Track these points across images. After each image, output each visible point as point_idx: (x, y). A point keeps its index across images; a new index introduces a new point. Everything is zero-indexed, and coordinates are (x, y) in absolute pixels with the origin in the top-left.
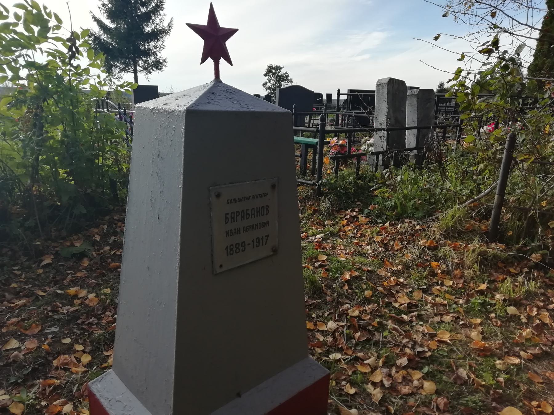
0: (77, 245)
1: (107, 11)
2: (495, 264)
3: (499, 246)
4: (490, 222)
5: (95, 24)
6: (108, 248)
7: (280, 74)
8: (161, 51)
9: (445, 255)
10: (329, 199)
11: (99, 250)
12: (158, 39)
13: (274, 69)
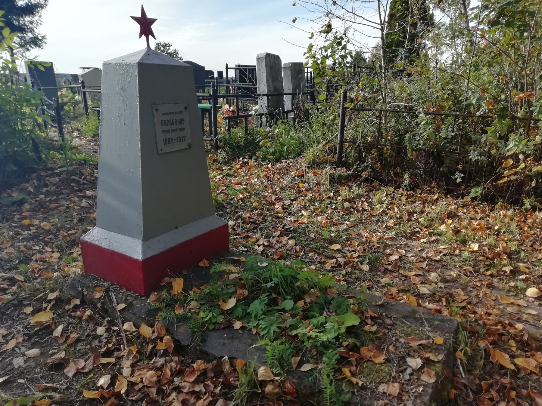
0: (15, 195)
2: (340, 182)
3: (342, 169)
6: (42, 196)
7: (169, 51)
8: (38, 27)
9: (308, 180)
10: (225, 151)
11: (35, 198)
12: (33, 14)
13: (162, 46)
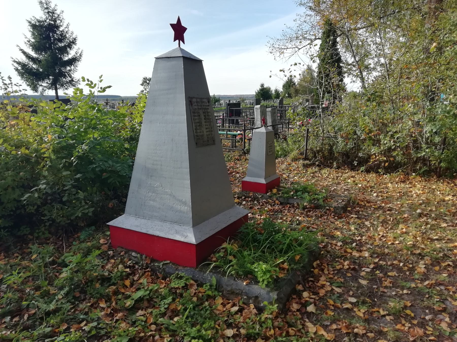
1: (31, 45)
4: (304, 155)
5: (22, 54)
